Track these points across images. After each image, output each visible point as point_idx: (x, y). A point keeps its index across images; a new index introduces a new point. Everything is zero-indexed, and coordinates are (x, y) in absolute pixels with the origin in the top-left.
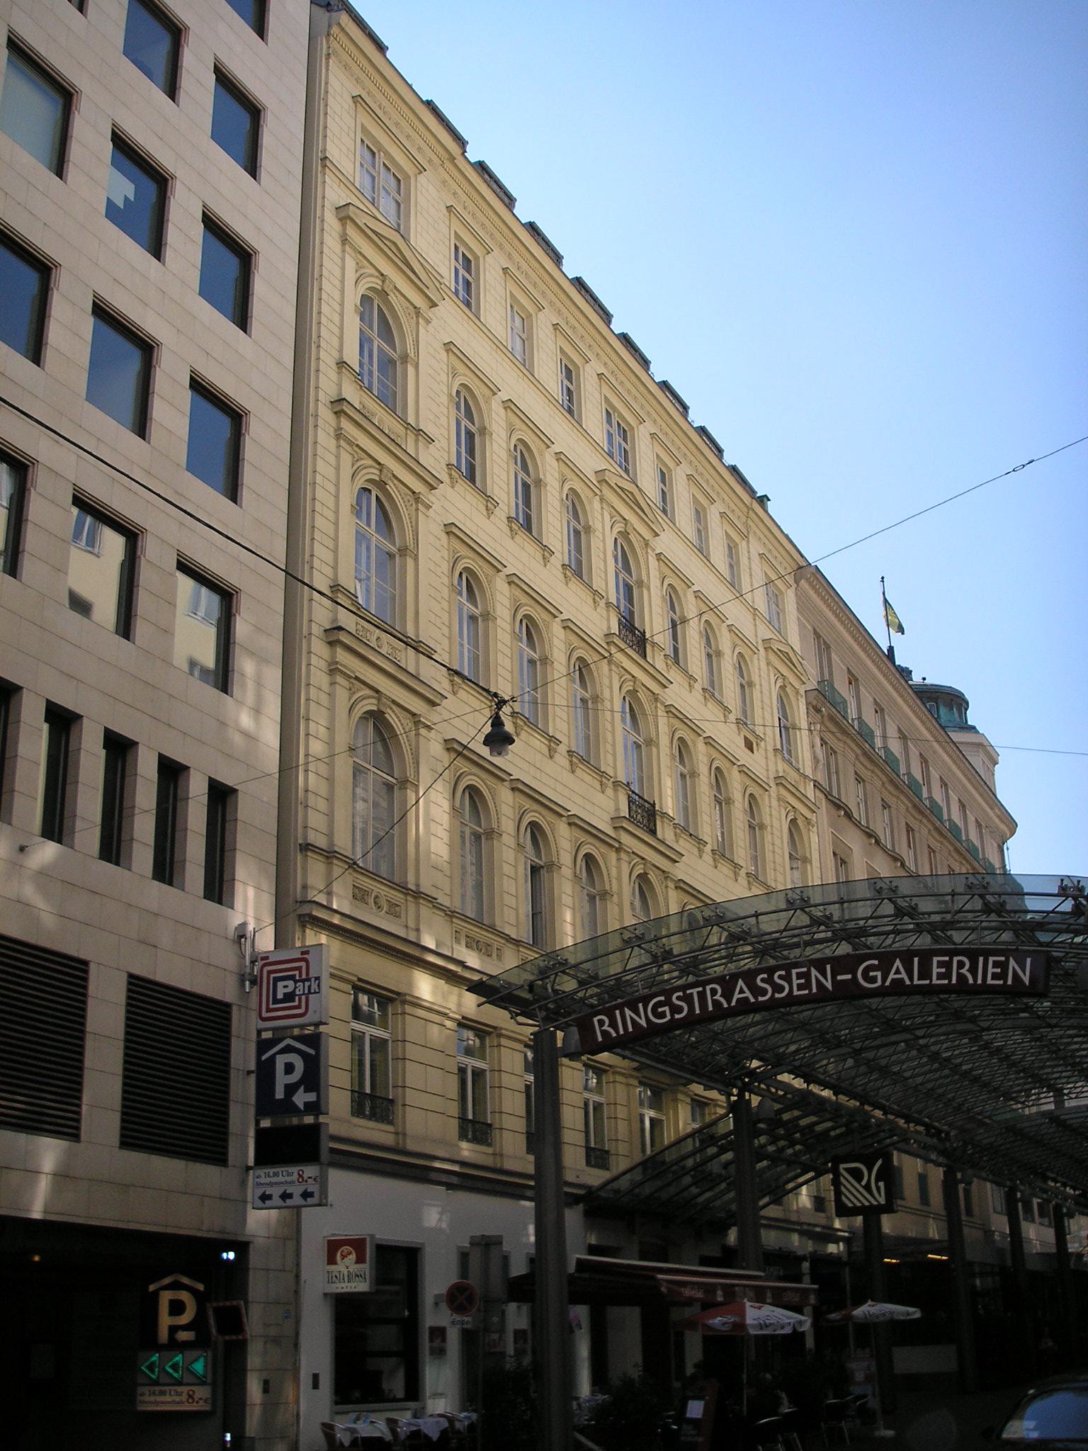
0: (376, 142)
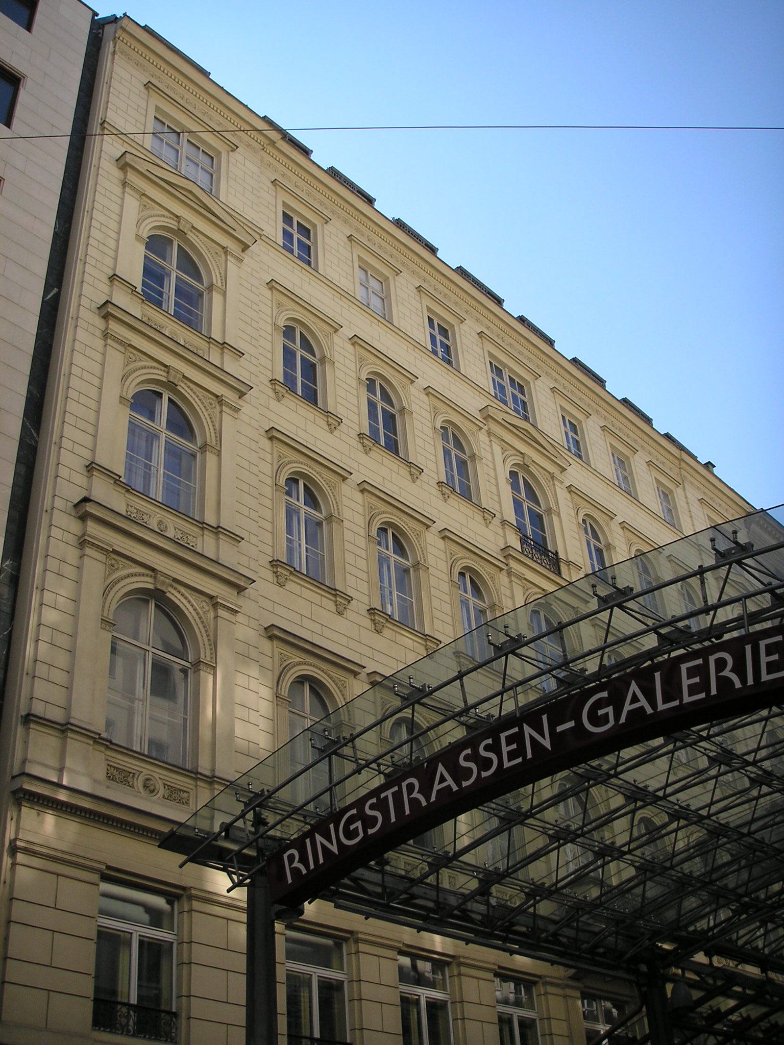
0: (178, 123)
